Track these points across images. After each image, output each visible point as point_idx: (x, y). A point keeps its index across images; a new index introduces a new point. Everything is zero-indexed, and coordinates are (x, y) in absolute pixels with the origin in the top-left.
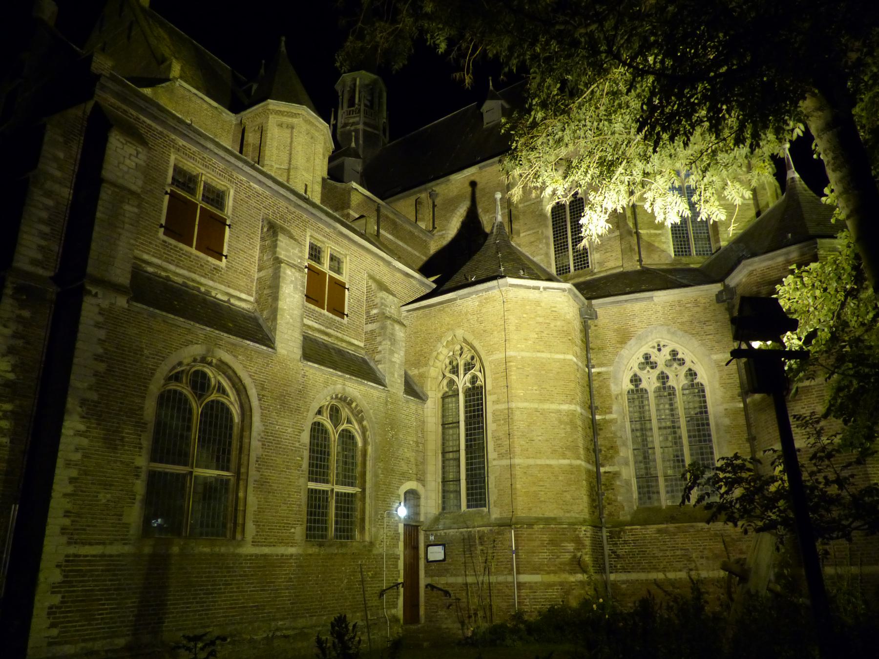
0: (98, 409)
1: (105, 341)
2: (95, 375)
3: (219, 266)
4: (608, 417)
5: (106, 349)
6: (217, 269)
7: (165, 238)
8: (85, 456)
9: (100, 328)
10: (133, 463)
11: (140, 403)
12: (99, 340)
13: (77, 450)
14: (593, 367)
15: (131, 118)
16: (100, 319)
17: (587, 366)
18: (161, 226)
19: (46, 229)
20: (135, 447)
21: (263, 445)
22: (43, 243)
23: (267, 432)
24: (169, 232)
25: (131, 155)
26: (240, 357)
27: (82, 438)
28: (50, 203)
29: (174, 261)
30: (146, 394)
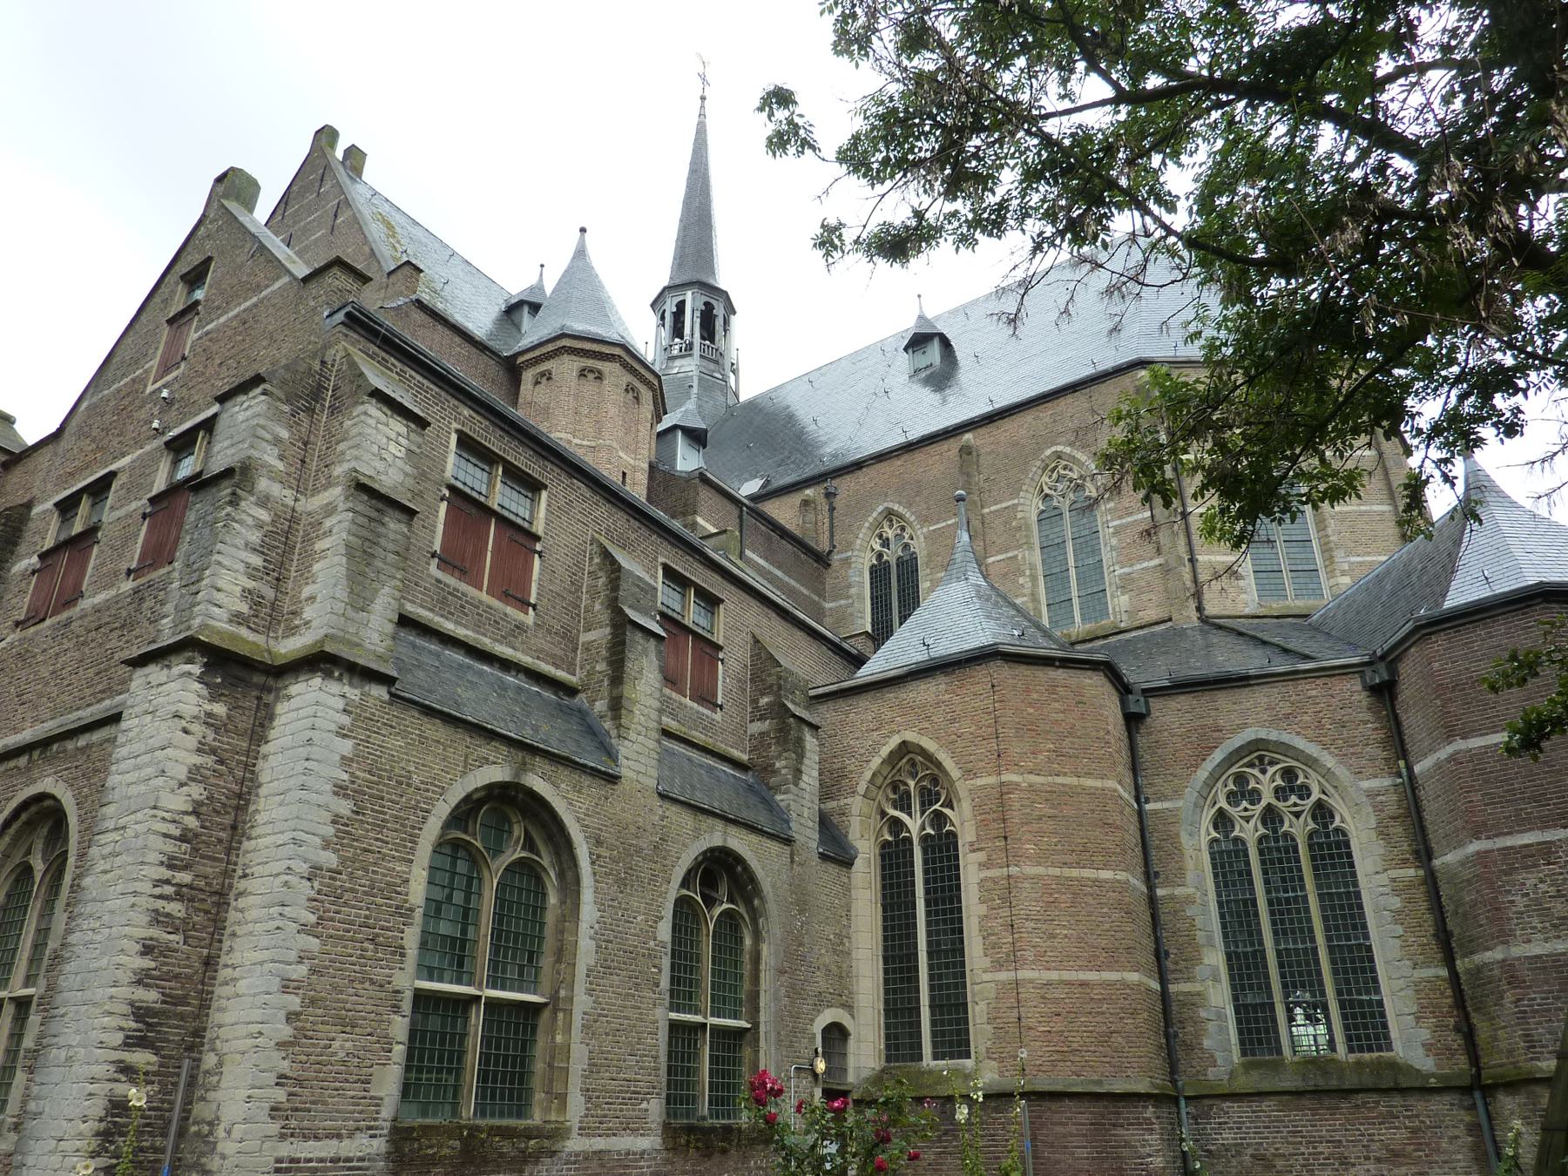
0: (338, 883)
1: (352, 760)
2: (334, 822)
3: (522, 623)
4: (1178, 891)
5: (352, 774)
6: (520, 627)
7: (440, 575)
8: (313, 971)
9: (345, 736)
10: (389, 983)
11: (404, 872)
12: (343, 757)
13: (300, 960)
14: (1147, 801)
15: (392, 371)
16: (346, 720)
17: (1137, 800)
18: (434, 555)
19: (257, 561)
20: (394, 953)
21: (598, 946)
22: (251, 584)
23: (605, 923)
24: (445, 562)
25: (399, 434)
26: (563, 786)
27: (311, 938)
28: (264, 516)
29: (453, 614)
30: (413, 854)
